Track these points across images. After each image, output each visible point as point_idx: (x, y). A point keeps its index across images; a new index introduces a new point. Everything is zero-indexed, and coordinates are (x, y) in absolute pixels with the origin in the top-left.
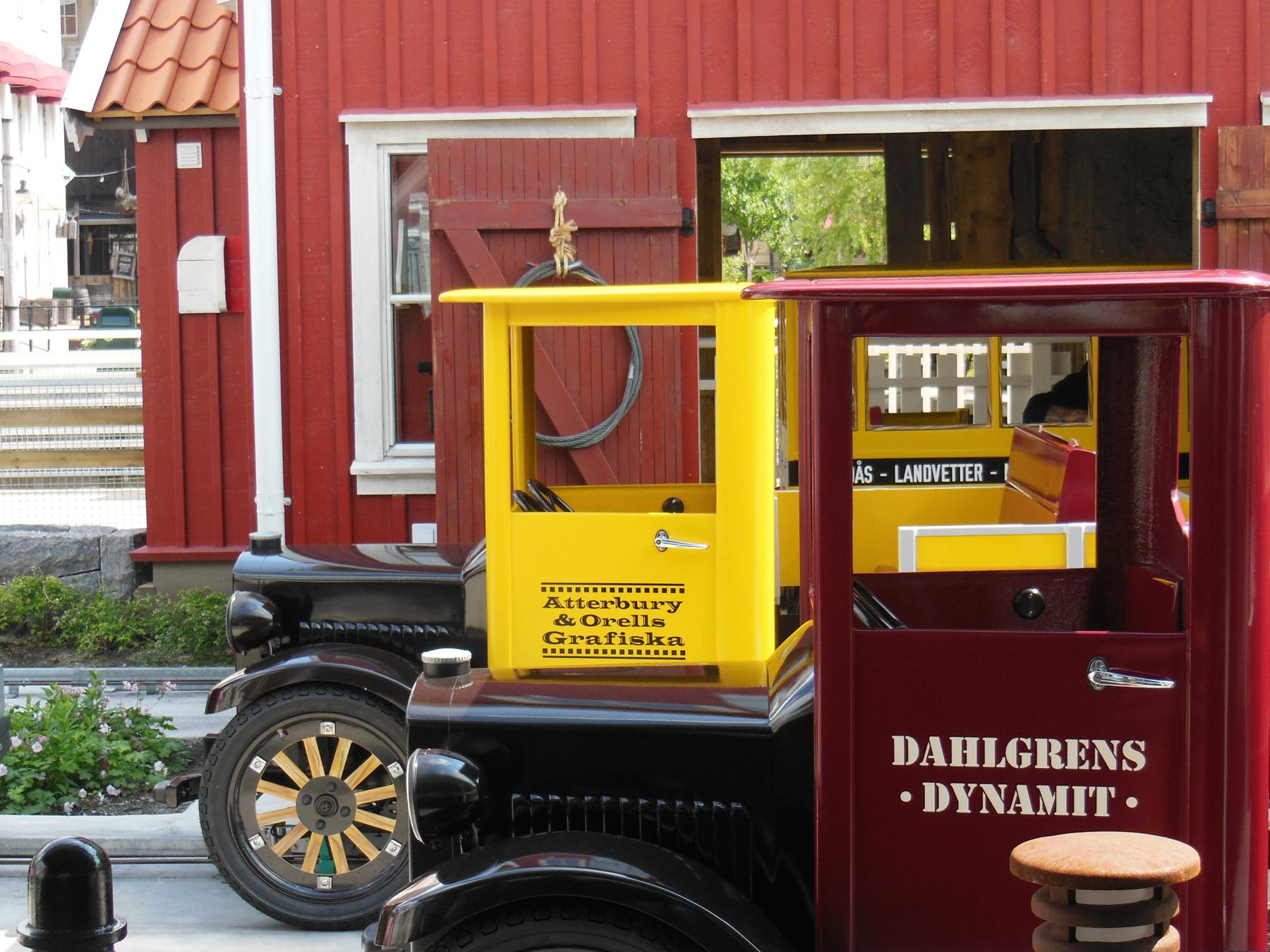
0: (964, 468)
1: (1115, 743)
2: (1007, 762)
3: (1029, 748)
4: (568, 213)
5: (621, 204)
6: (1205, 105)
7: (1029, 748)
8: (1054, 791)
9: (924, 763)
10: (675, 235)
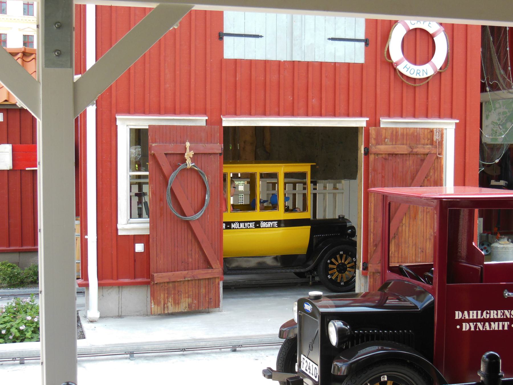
0: (275, 223)
1: (509, 311)
2: (483, 317)
3: (489, 313)
4: (191, 149)
5: (205, 146)
6: (366, 121)
7: (489, 313)
8: (494, 323)
9: (463, 318)
10: (219, 155)
